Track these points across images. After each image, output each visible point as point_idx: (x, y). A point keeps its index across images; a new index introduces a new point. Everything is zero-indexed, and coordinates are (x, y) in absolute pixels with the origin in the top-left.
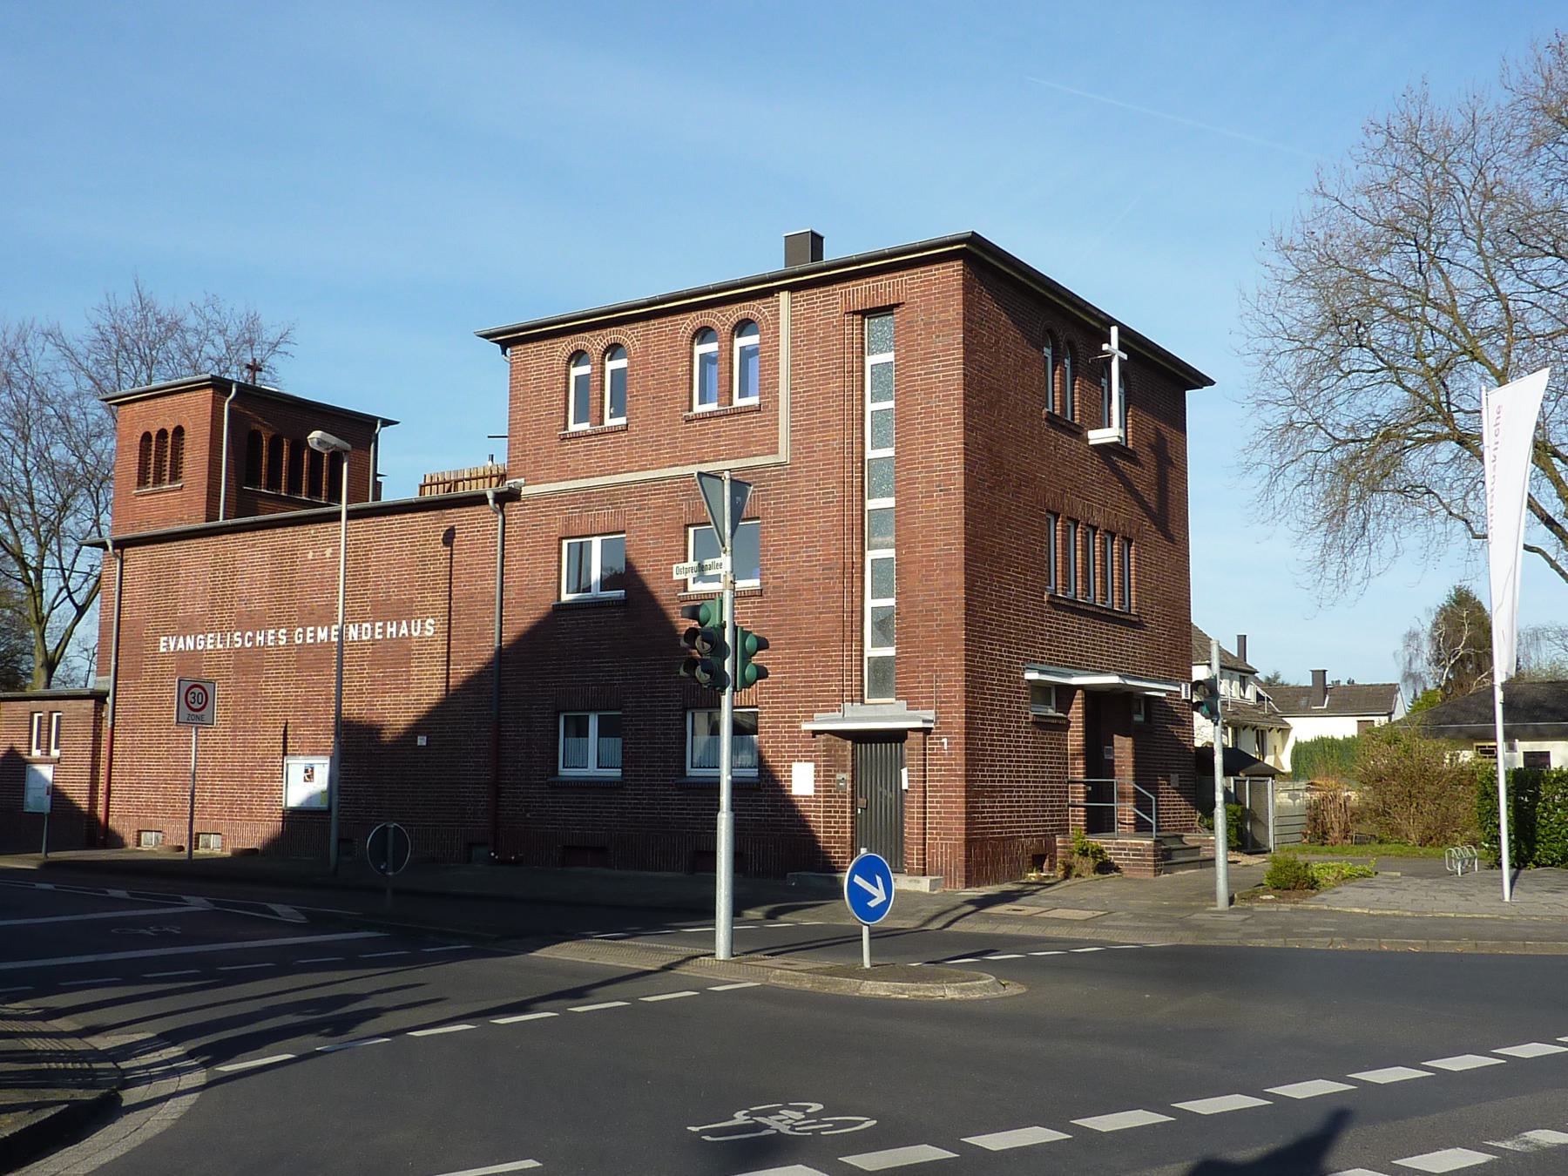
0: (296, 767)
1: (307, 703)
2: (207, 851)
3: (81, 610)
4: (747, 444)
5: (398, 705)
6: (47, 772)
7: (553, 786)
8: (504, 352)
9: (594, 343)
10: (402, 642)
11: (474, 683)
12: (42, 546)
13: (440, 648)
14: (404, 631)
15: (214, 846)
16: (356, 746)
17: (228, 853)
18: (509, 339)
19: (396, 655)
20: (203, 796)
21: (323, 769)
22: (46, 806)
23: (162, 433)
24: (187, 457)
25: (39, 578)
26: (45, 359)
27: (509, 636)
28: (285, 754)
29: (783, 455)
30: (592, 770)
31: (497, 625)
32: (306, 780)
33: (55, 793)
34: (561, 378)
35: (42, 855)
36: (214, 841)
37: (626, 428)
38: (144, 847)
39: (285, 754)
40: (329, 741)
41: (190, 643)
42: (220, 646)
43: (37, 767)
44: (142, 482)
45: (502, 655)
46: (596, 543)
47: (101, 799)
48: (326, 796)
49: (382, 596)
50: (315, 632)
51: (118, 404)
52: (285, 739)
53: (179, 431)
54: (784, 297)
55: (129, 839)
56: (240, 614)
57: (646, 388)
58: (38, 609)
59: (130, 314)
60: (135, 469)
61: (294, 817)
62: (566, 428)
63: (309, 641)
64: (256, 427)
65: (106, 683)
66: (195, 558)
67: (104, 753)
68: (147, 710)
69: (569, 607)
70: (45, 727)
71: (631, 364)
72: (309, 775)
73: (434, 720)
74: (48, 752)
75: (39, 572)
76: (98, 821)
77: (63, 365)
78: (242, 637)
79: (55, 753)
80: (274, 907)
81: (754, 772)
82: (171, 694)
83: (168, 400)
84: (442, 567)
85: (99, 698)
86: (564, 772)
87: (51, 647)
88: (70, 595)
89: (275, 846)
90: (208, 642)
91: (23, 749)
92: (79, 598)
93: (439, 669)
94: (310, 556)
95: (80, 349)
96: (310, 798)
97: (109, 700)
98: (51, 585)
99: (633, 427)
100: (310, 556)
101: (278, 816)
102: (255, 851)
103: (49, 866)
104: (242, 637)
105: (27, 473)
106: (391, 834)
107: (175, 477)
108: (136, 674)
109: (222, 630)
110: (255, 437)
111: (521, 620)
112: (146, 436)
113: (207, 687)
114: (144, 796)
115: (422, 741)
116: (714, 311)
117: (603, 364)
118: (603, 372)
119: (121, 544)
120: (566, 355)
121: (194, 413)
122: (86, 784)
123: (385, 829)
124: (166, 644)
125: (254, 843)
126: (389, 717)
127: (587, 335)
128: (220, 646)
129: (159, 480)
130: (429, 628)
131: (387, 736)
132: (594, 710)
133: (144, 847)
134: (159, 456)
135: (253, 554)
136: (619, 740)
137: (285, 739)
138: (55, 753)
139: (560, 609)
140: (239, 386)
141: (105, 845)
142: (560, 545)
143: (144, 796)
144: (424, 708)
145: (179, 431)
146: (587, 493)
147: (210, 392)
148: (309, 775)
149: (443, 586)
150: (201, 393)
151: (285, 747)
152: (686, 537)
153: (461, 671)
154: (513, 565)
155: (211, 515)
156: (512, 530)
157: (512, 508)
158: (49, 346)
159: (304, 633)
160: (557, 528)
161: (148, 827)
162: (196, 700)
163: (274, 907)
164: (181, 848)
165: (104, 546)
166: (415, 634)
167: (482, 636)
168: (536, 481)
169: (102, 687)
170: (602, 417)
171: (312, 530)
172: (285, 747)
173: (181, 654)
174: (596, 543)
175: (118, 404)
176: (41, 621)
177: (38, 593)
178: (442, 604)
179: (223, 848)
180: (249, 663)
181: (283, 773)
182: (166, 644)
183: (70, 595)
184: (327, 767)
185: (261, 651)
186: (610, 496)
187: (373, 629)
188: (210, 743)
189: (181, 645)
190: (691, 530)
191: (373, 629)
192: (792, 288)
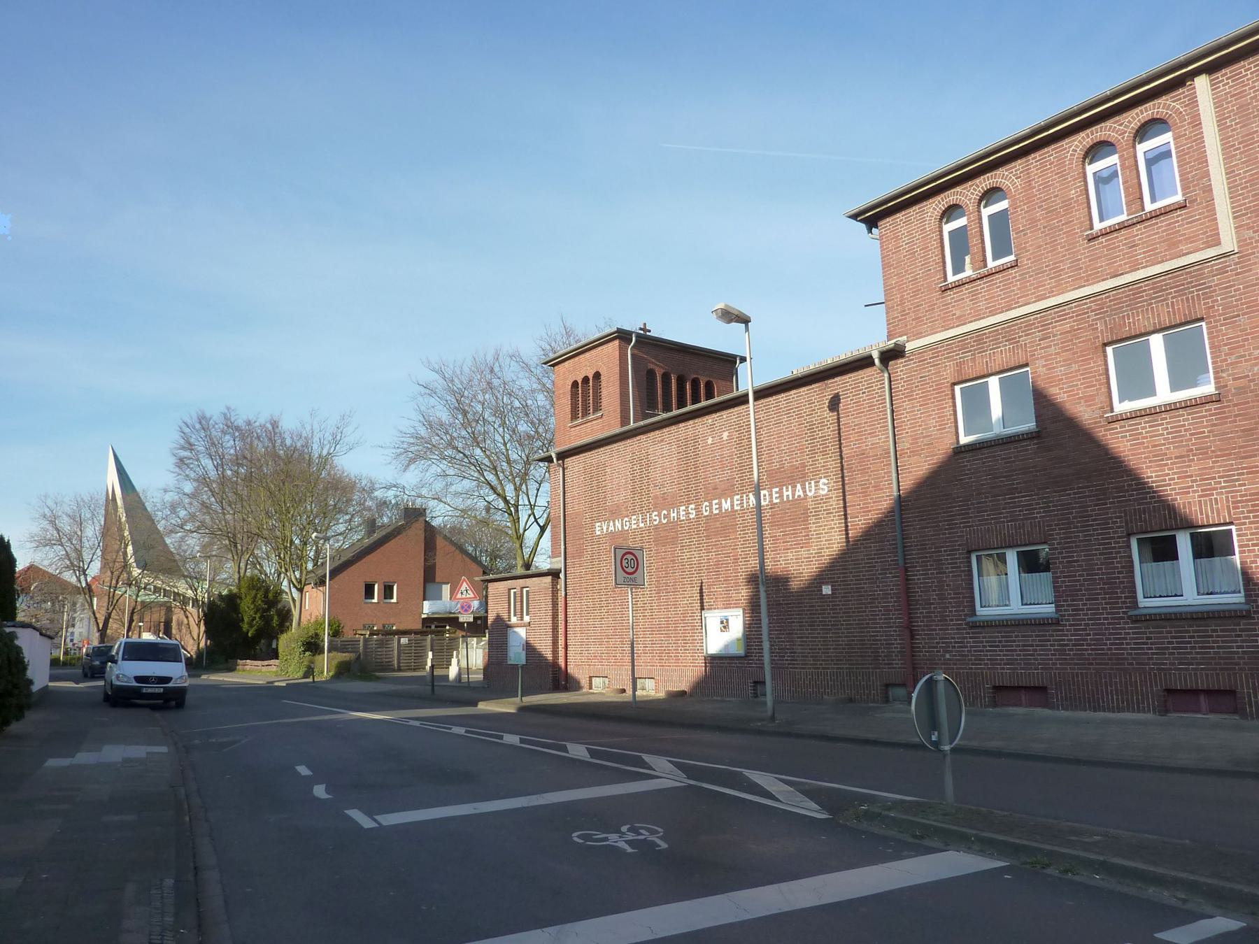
0: (712, 619)
1: (717, 564)
2: (644, 693)
3: (543, 529)
4: (1173, 245)
5: (805, 556)
6: (522, 632)
7: (974, 626)
8: (870, 231)
9: (967, 194)
10: (797, 502)
11: (874, 532)
12: (517, 489)
13: (836, 504)
14: (799, 492)
15: (650, 690)
16: (771, 597)
17: (662, 695)
18: (872, 218)
19: (798, 514)
20: (639, 648)
21: (738, 623)
22: (522, 660)
23: (586, 380)
24: (604, 392)
25: (517, 511)
26: (511, 371)
27: (908, 483)
28: (702, 609)
29: (1229, 242)
30: (1016, 608)
31: (894, 475)
32: (723, 630)
33: (529, 648)
34: (935, 236)
35: (517, 700)
36: (650, 684)
37: (1014, 265)
38: (594, 690)
39: (702, 609)
40: (744, 593)
41: (618, 525)
42: (642, 525)
43: (517, 630)
44: (574, 416)
45: (902, 503)
46: (994, 383)
47: (561, 653)
48: (742, 644)
49: (776, 466)
50: (720, 504)
51: (553, 366)
52: (702, 596)
53: (597, 376)
54: (1202, 82)
55: (584, 682)
56: (656, 497)
57: (1033, 221)
58: (517, 531)
59: (559, 338)
60: (568, 409)
61: (715, 661)
62: (946, 280)
63: (716, 512)
64: (651, 366)
65: (558, 563)
66: (616, 459)
67: (561, 616)
68: (593, 576)
69: (971, 448)
70: (518, 604)
71: (1013, 205)
72: (725, 625)
73: (835, 570)
74: (522, 618)
75: (516, 506)
76: (560, 668)
77: (521, 375)
78: (659, 515)
79: (527, 619)
80: (757, 777)
81: (1238, 598)
82: (608, 565)
83: (587, 355)
84: (830, 431)
85: (554, 574)
86: (982, 612)
87: (526, 556)
88: (536, 520)
89: (702, 687)
90: (632, 523)
91: (505, 616)
92: (542, 522)
93: (837, 523)
94: (710, 441)
95: (531, 363)
96: (726, 646)
97: (562, 575)
98: (524, 515)
99: (1024, 261)
100: (710, 441)
101: (701, 662)
102: (683, 693)
103: (524, 709)
104: (659, 515)
105: (505, 444)
106: (941, 688)
107: (597, 409)
108: (580, 554)
109: (643, 511)
110: (651, 373)
111: (918, 468)
112: (575, 384)
113: (637, 553)
114: (593, 649)
115: (827, 590)
116: (1108, 123)
117: (979, 211)
118: (980, 219)
119: (563, 456)
120: (938, 213)
121: (607, 360)
122: (550, 642)
123: (931, 683)
124: (601, 528)
125: (684, 686)
126: (792, 569)
127: (958, 189)
128: (642, 525)
129: (586, 413)
130: (823, 487)
131: (795, 585)
132: (1010, 547)
133: (594, 690)
134: (585, 395)
135: (662, 449)
136: (1049, 574)
137: (702, 596)
138: (527, 619)
139: (960, 451)
140: (638, 336)
141: (566, 689)
142: (953, 390)
143: (593, 649)
144: (825, 560)
145: (597, 376)
146: (978, 335)
147: (617, 342)
148: (725, 625)
149: (833, 448)
150: (611, 344)
151: (702, 603)
152: (1105, 356)
153: (859, 523)
154: (904, 417)
155: (624, 420)
156: (899, 386)
157: (897, 365)
158: (513, 363)
159: (711, 506)
160: (949, 373)
161: (600, 680)
162: (629, 563)
163: (757, 777)
164: (624, 691)
165: (549, 459)
166: (810, 494)
167: (877, 488)
168: (919, 335)
169: (556, 566)
170: (984, 260)
171: (709, 419)
172: (702, 603)
173: (612, 535)
174: (994, 383)
175: (553, 366)
176: (520, 538)
177: (516, 521)
178: (833, 464)
179: (657, 690)
180: (667, 535)
181: (702, 624)
182: (601, 528)
183: (536, 520)
184: (741, 618)
185: (673, 526)
186: (1006, 332)
187: (771, 495)
188: (640, 604)
189: (611, 528)
190: (1109, 350)
191: (771, 495)
192: (1210, 69)
